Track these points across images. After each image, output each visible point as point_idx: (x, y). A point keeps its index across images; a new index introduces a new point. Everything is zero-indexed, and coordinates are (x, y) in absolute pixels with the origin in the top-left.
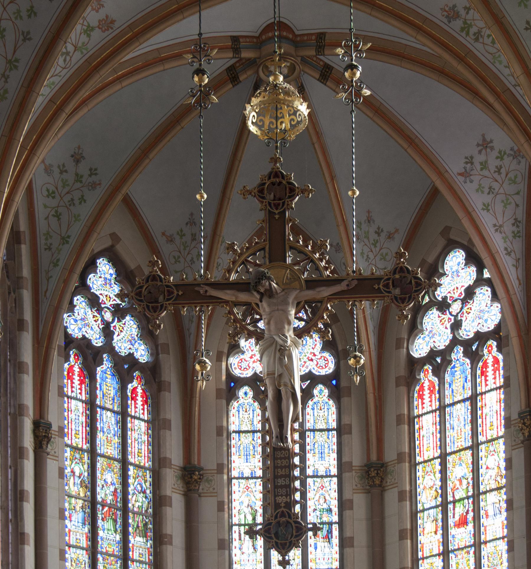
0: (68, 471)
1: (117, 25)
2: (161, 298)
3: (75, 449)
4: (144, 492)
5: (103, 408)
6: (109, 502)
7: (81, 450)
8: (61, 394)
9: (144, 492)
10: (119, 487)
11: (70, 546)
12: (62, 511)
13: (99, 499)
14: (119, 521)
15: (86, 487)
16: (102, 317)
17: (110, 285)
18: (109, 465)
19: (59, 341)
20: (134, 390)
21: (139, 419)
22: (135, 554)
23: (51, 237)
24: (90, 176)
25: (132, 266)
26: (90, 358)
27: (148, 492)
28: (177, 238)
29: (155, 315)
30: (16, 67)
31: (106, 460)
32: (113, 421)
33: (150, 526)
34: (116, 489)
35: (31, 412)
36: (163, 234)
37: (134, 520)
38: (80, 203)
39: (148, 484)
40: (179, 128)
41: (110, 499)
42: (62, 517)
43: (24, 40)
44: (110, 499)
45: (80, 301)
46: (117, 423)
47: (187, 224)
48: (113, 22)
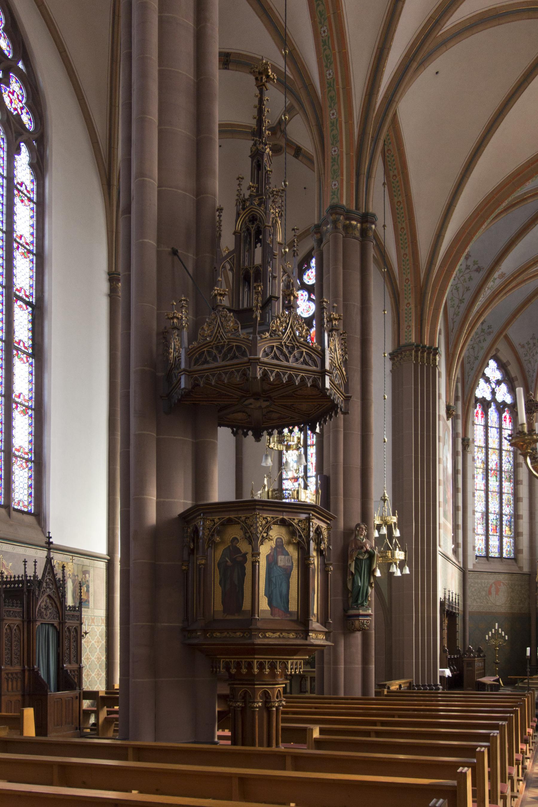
0: (476, 458)
1: (506, 275)
2: (533, 408)
3: (479, 447)
4: (509, 462)
5: (491, 427)
6: (493, 468)
7: (482, 447)
8: (473, 424)
9: (509, 462)
10: (498, 461)
11: (476, 490)
12: (473, 476)
13: (489, 467)
14: (498, 476)
15: (484, 463)
16: (491, 386)
17: (495, 371)
18: (494, 452)
19: (473, 401)
20: (505, 417)
21: (507, 429)
22: (505, 490)
23: (470, 358)
24: (488, 329)
25: (505, 361)
26: (486, 406)
27: (511, 461)
28: (526, 345)
29: (531, 415)
30: (463, 302)
31: (492, 450)
32: (496, 432)
33: (512, 477)
34: (497, 463)
35: (461, 435)
36: (519, 344)
37: (505, 475)
38: (484, 341)
39: (511, 458)
40: (530, 303)
41: (494, 467)
42: (474, 478)
43: (467, 291)
44: (494, 467)
45: (482, 381)
46: (498, 432)
47: (531, 339)
48: (505, 274)
